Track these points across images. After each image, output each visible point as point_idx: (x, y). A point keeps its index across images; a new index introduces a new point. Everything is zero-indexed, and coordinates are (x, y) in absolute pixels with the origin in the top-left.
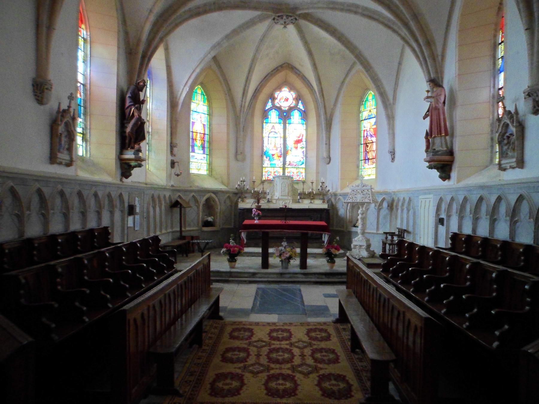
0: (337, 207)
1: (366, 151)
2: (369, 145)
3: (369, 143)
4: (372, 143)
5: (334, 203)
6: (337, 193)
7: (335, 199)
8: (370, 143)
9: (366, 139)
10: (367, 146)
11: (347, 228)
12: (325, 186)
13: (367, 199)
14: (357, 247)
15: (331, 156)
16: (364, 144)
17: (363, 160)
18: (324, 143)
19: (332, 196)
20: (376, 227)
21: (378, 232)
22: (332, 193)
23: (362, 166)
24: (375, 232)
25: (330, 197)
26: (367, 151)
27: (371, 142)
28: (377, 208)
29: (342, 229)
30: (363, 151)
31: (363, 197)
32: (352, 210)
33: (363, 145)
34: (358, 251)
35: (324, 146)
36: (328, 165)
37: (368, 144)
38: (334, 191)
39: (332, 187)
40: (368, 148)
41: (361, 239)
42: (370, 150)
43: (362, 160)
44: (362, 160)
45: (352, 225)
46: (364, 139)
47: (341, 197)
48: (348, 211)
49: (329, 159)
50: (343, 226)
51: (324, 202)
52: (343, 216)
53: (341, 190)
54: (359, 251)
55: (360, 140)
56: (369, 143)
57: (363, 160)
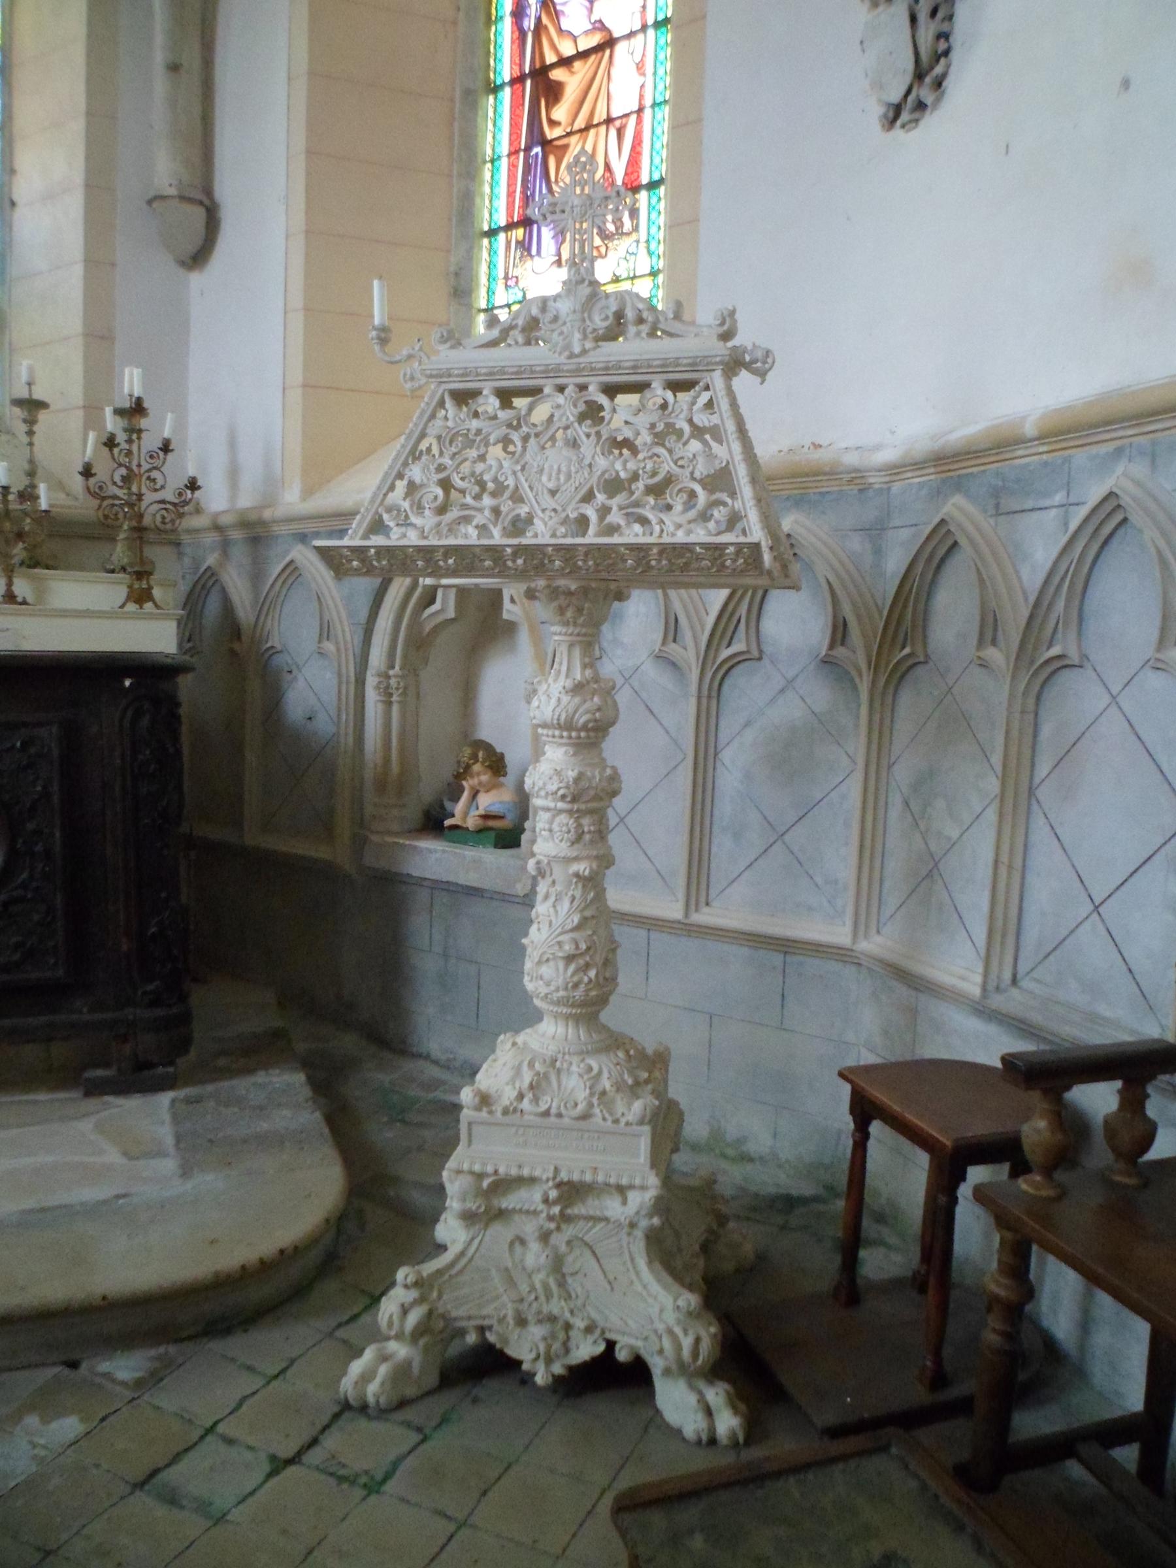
0: (275, 641)
1: (537, 137)
2: (572, 81)
3: (565, 62)
4: (598, 49)
5: (244, 612)
6: (267, 514)
7: (256, 576)
8: (583, 55)
9: (539, 27)
10: (551, 92)
11: (359, 843)
12: (151, 442)
13: (677, 514)
14: (533, 1197)
15: (227, 189)
16: (517, 81)
17: (510, 227)
18: (159, 58)
19: (225, 546)
20: (679, 860)
21: (704, 917)
22: (225, 520)
23: (500, 287)
24: (673, 910)
25: (211, 560)
26: (551, 134)
27: (595, 40)
28: (689, 653)
29: (321, 852)
30: (504, 149)
31: (614, 486)
32: (412, 670)
33: (506, 94)
34: (534, 1255)
35: (160, 85)
36: (196, 280)
37: (557, 74)
38: (245, 501)
39: (234, 473)
40: (560, 112)
41: (575, 1086)
42: (580, 123)
43: (492, 233)
44: (492, 233)
45: (413, 812)
46: (521, 34)
47: (304, 556)
48: (371, 681)
49: (199, 213)
50: (326, 828)
51: (141, 596)
52: (324, 725)
53: (308, 492)
54: (557, 1265)
55: (481, 49)
56: (565, 62)
57: (510, 227)
